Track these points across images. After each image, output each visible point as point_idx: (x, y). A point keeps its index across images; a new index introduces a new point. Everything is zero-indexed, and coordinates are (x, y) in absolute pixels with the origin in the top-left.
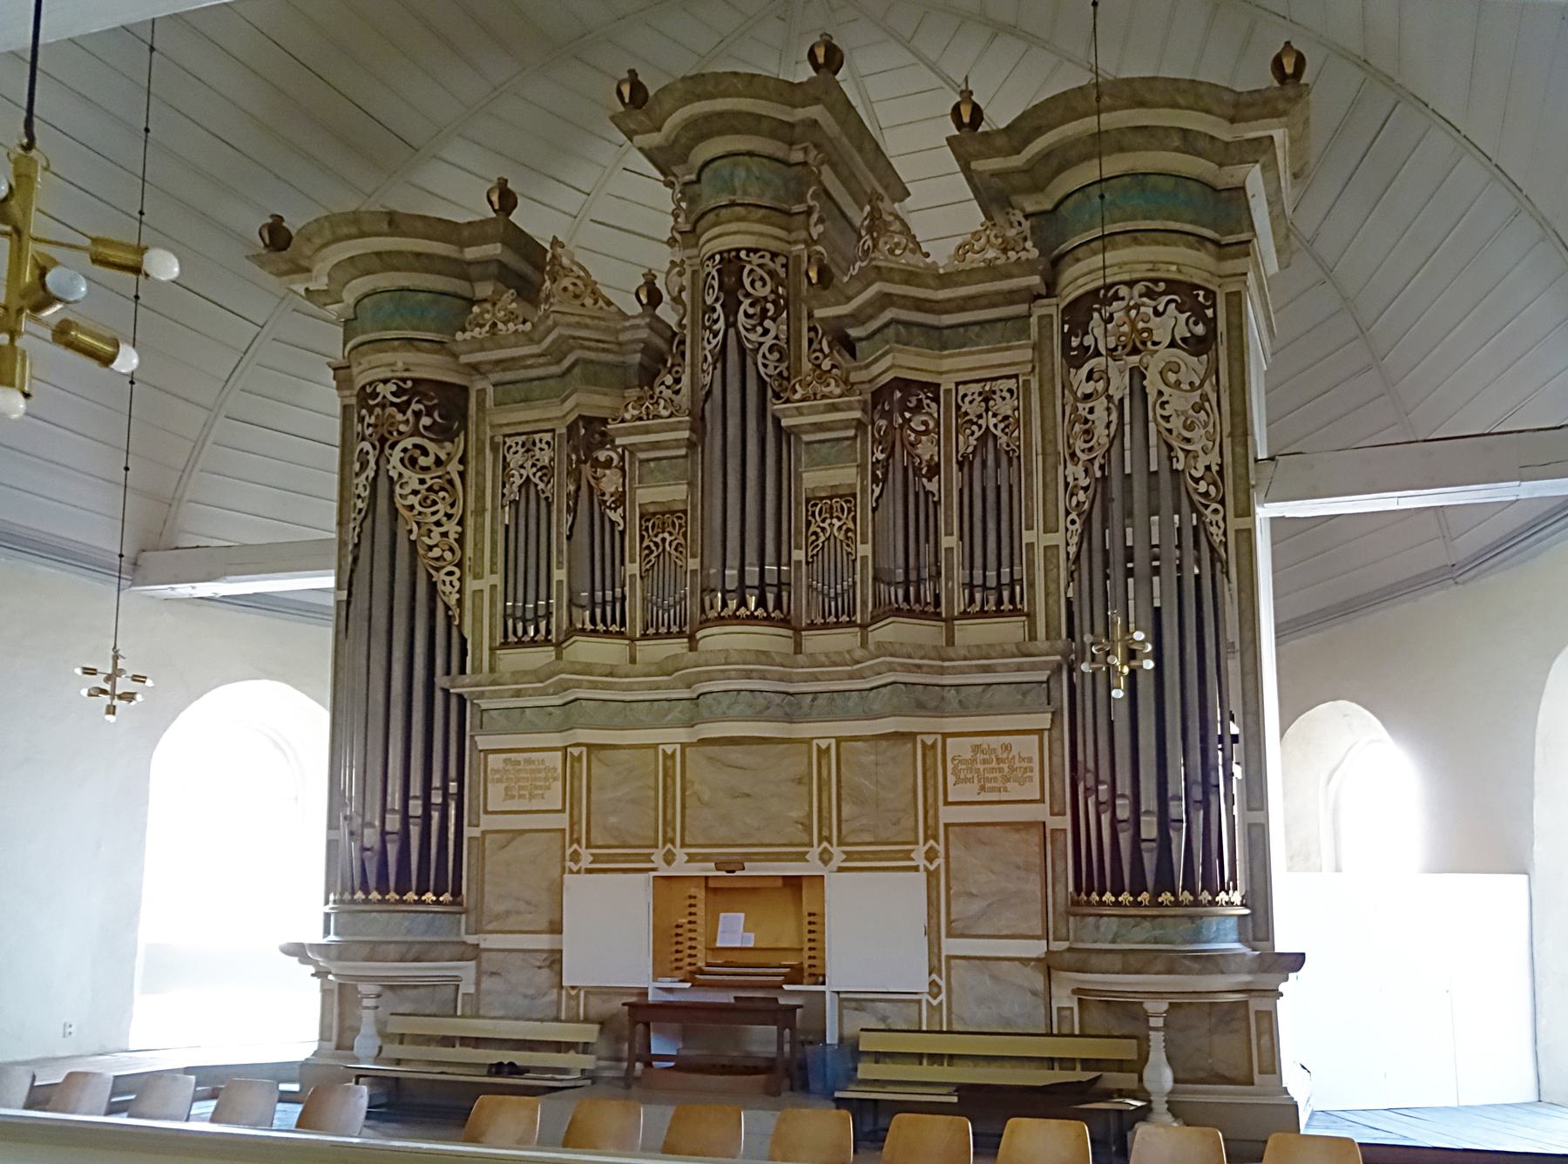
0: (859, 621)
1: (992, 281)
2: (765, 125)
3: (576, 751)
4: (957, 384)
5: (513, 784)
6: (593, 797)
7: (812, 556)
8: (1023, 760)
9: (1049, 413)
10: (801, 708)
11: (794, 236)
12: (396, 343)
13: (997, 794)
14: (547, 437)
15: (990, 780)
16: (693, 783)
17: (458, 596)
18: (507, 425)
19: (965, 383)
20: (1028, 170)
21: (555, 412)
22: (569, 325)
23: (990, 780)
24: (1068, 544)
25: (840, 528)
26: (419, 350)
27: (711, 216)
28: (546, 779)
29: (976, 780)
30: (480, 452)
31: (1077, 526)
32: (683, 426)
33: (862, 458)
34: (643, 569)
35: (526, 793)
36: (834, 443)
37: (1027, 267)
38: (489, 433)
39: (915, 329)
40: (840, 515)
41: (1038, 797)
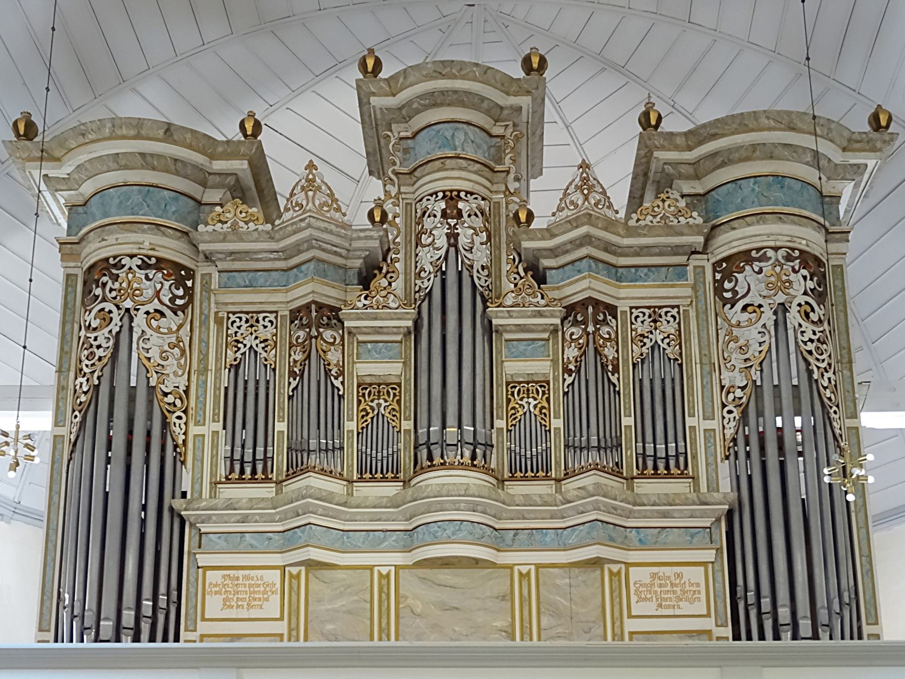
0: (553, 476)
1: (667, 236)
2: (485, 105)
3: (294, 570)
4: (631, 308)
5: (231, 596)
6: (310, 609)
7: (363, 428)
8: (692, 585)
9: (704, 334)
10: (503, 540)
11: (494, 188)
12: (146, 226)
13: (672, 610)
14: (272, 317)
15: (666, 600)
16: (406, 598)
17: (184, 437)
18: (232, 304)
19: (637, 308)
20: (695, 164)
21: (279, 297)
22: (318, 229)
23: (666, 600)
24: (71, 433)
25: (535, 406)
26: (164, 234)
27: (438, 163)
28: (265, 592)
29: (654, 599)
30: (204, 323)
31: (735, 414)
32: (409, 316)
33: (553, 354)
34: (360, 427)
35: (245, 604)
36: (530, 342)
37: (696, 230)
38: (213, 309)
39: (601, 265)
40: (536, 396)
41: (705, 613)
